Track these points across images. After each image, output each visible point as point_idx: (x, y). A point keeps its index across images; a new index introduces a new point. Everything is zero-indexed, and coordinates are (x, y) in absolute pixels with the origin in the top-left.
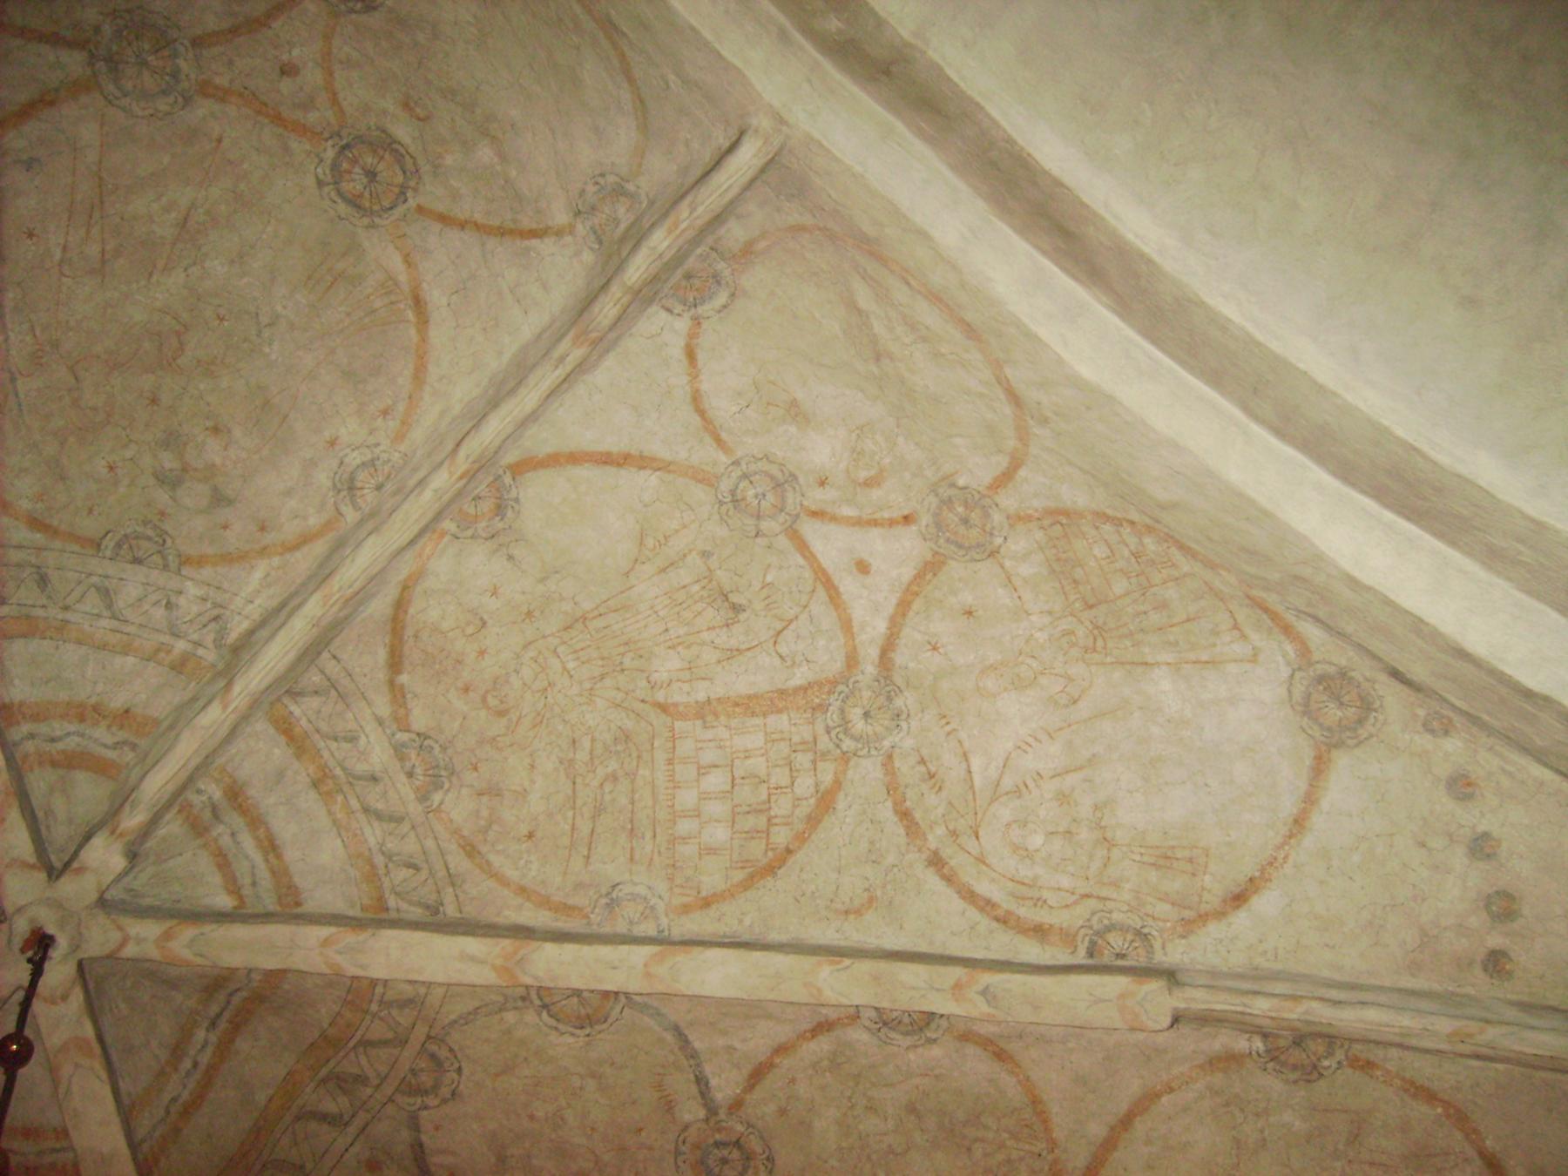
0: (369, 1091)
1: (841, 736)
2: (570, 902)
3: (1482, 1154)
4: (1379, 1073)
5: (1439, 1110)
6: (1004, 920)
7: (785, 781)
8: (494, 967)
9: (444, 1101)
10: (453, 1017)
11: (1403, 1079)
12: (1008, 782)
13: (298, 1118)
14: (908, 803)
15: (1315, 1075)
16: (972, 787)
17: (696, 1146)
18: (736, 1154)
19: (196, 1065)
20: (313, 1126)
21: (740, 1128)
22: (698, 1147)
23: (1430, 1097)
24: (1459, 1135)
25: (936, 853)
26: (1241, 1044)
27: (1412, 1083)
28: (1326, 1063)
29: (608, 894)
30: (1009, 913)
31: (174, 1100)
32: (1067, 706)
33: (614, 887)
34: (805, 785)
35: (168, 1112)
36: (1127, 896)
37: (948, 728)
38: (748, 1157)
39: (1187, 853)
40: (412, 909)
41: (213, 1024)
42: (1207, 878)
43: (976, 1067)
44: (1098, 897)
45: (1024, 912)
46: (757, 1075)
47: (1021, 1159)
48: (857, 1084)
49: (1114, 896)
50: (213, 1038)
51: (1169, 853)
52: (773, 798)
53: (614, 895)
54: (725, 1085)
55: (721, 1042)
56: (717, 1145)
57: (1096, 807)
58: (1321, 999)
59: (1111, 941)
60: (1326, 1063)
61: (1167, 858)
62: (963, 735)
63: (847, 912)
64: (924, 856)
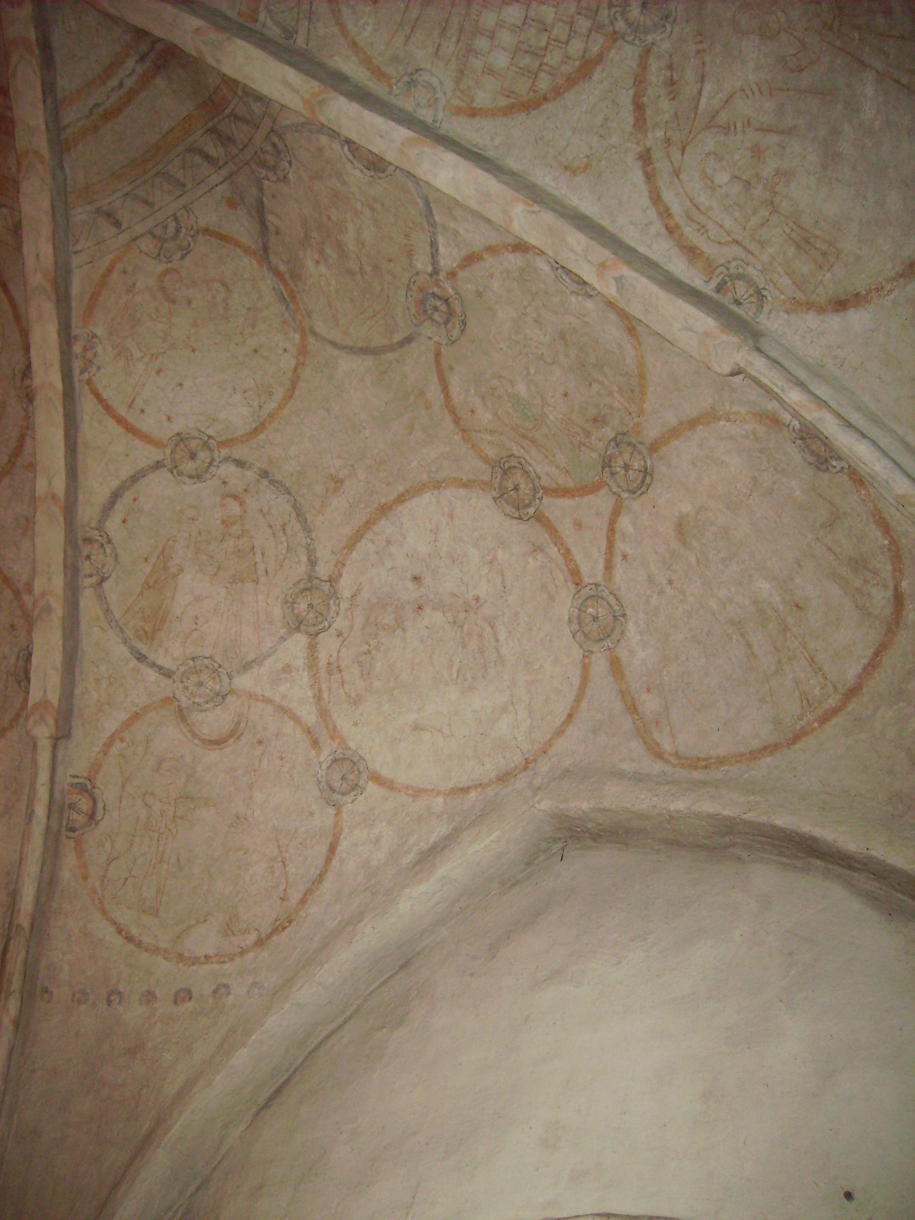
0: (236, 151)
1: (618, 15)
2: (385, 69)
3: (896, 588)
4: (863, 492)
5: (886, 542)
6: (672, 231)
7: (563, 37)
8: (302, 98)
9: (279, 180)
10: (288, 122)
11: (875, 506)
12: (723, 117)
13: (189, 150)
14: (645, 99)
15: (823, 467)
16: (696, 108)
17: (421, 290)
18: (443, 308)
19: (121, 85)
20: (198, 159)
21: (451, 291)
22: (422, 291)
23: (886, 529)
24: (889, 567)
25: (648, 150)
26: (786, 417)
27: (880, 512)
28: (834, 463)
29: (412, 74)
30: (677, 226)
31: (97, 105)
32: (793, 71)
33: (417, 70)
34: (576, 47)
35: (91, 113)
36: (765, 258)
37: (700, 47)
38: (451, 314)
39: (824, 247)
40: (275, 28)
41: (142, 59)
42: (828, 275)
43: (612, 332)
44: (745, 248)
45: (689, 232)
46: (470, 259)
47: (619, 410)
48: (533, 300)
49: (756, 253)
50: (140, 70)
51: (812, 240)
52: (550, 47)
53: (415, 77)
54: (448, 257)
55: (452, 225)
56: (434, 295)
57: (777, 173)
58: (839, 416)
59: (737, 286)
60: (834, 463)
61: (809, 243)
62: (708, 58)
63: (566, 168)
64: (639, 149)
